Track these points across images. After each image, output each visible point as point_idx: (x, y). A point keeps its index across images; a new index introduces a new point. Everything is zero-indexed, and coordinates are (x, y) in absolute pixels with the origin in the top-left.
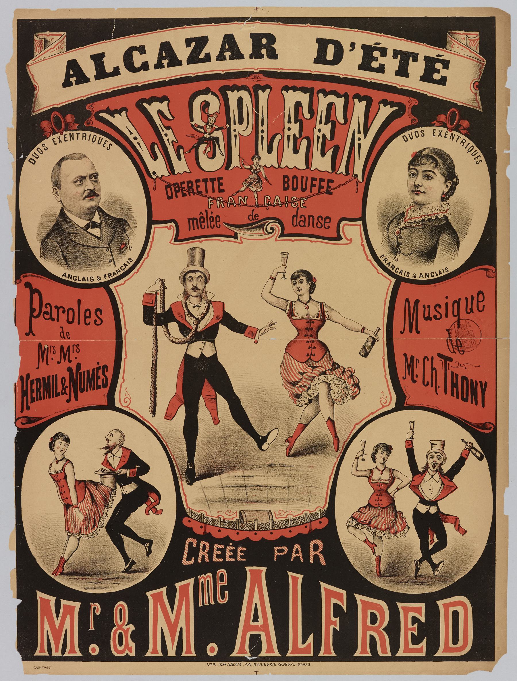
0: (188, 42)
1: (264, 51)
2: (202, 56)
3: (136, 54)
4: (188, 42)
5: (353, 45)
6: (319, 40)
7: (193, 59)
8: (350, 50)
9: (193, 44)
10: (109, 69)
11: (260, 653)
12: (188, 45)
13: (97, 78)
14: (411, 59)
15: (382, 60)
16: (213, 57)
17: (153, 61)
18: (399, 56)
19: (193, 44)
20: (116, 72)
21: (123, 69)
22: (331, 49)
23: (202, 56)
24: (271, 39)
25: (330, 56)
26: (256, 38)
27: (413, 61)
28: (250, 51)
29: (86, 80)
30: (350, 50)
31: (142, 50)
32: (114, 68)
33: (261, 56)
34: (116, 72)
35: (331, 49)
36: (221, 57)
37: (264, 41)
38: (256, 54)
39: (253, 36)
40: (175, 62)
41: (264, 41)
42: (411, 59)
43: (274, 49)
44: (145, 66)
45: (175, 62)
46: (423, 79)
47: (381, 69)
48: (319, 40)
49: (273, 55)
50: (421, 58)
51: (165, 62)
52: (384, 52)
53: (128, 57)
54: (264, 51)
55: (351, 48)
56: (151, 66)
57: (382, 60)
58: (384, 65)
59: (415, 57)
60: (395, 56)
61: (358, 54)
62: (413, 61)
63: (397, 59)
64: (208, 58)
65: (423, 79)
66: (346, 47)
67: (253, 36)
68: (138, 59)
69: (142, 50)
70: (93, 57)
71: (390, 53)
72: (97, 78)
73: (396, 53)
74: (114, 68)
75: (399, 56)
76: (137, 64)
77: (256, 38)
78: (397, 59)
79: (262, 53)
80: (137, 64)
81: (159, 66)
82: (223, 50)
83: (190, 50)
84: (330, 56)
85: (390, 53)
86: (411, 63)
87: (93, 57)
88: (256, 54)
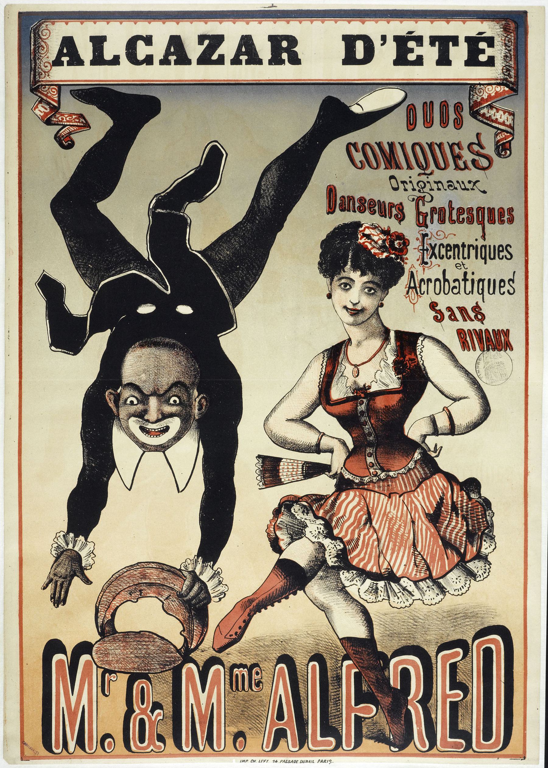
0: (201, 39)
1: (285, 56)
2: (215, 57)
3: (140, 44)
4: (201, 39)
5: (384, 38)
6: (345, 38)
7: (204, 59)
8: (382, 45)
9: (207, 42)
10: (108, 56)
11: (295, 47)
12: (201, 42)
13: (93, 63)
14: (451, 43)
15: (418, 51)
16: (227, 60)
17: (159, 55)
18: (437, 43)
19: (207, 42)
20: (116, 61)
21: (123, 59)
22: (360, 46)
23: (215, 57)
24: (292, 41)
25: (360, 54)
26: (275, 40)
27: (453, 46)
28: (270, 57)
29: (80, 62)
30: (382, 45)
31: (148, 40)
32: (114, 56)
33: (282, 62)
34: (116, 61)
35: (360, 46)
36: (236, 61)
37: (285, 44)
38: (276, 60)
39: (272, 38)
40: (184, 60)
41: (285, 44)
42: (451, 43)
43: (296, 53)
44: (149, 60)
45: (184, 60)
46: (468, 63)
47: (419, 61)
48: (345, 38)
49: (295, 60)
50: (461, 40)
51: (173, 58)
52: (419, 40)
53: (131, 45)
54: (285, 56)
55: (382, 42)
56: (156, 61)
57: (418, 51)
58: (422, 56)
59: (455, 40)
60: (432, 44)
61: (391, 49)
62: (453, 46)
63: (435, 46)
64: (221, 60)
65: (468, 63)
66: (377, 42)
67: (272, 38)
68: (142, 51)
69: (148, 40)
70: (93, 39)
71: (426, 41)
72: (93, 63)
73: (433, 40)
74: (114, 56)
75: (437, 43)
76: (141, 56)
77: (275, 40)
78: (435, 46)
79: (283, 58)
80: (141, 56)
81: (165, 62)
82: (239, 52)
83: (202, 48)
84: (360, 54)
85: (426, 41)
86: (452, 50)
87: (93, 39)
88: (276, 60)
